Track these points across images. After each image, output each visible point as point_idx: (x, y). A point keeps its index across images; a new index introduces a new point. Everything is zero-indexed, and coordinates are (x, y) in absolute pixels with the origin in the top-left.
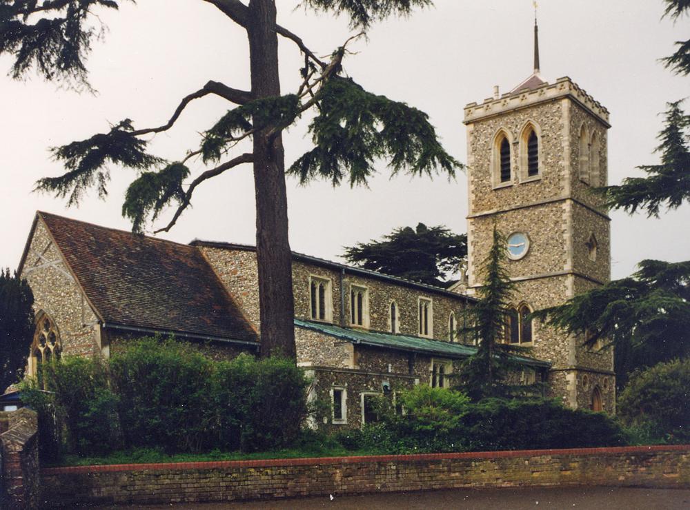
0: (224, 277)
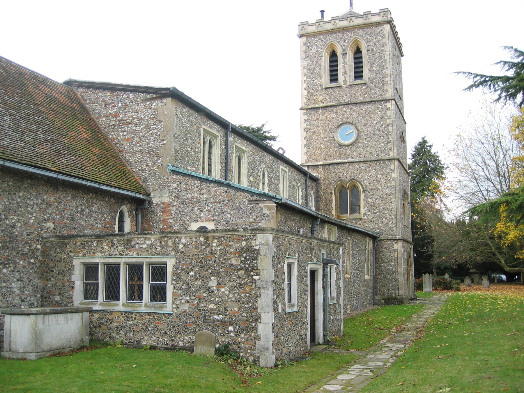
0: (102, 120)
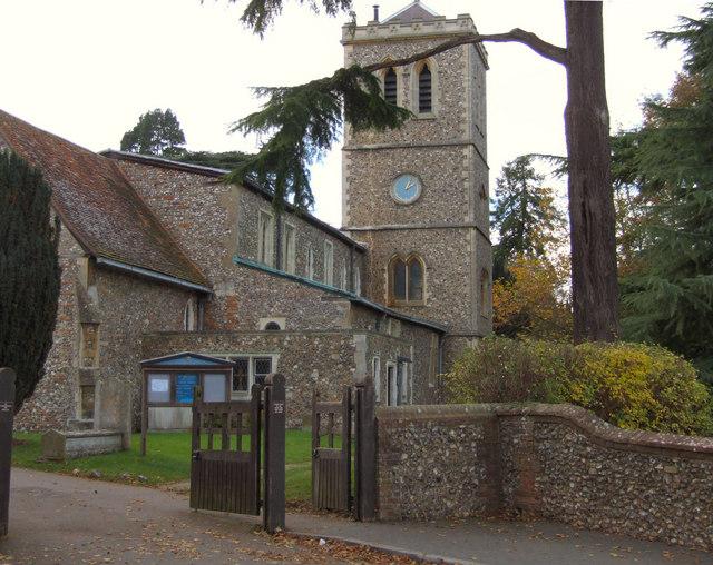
0: (151, 202)
